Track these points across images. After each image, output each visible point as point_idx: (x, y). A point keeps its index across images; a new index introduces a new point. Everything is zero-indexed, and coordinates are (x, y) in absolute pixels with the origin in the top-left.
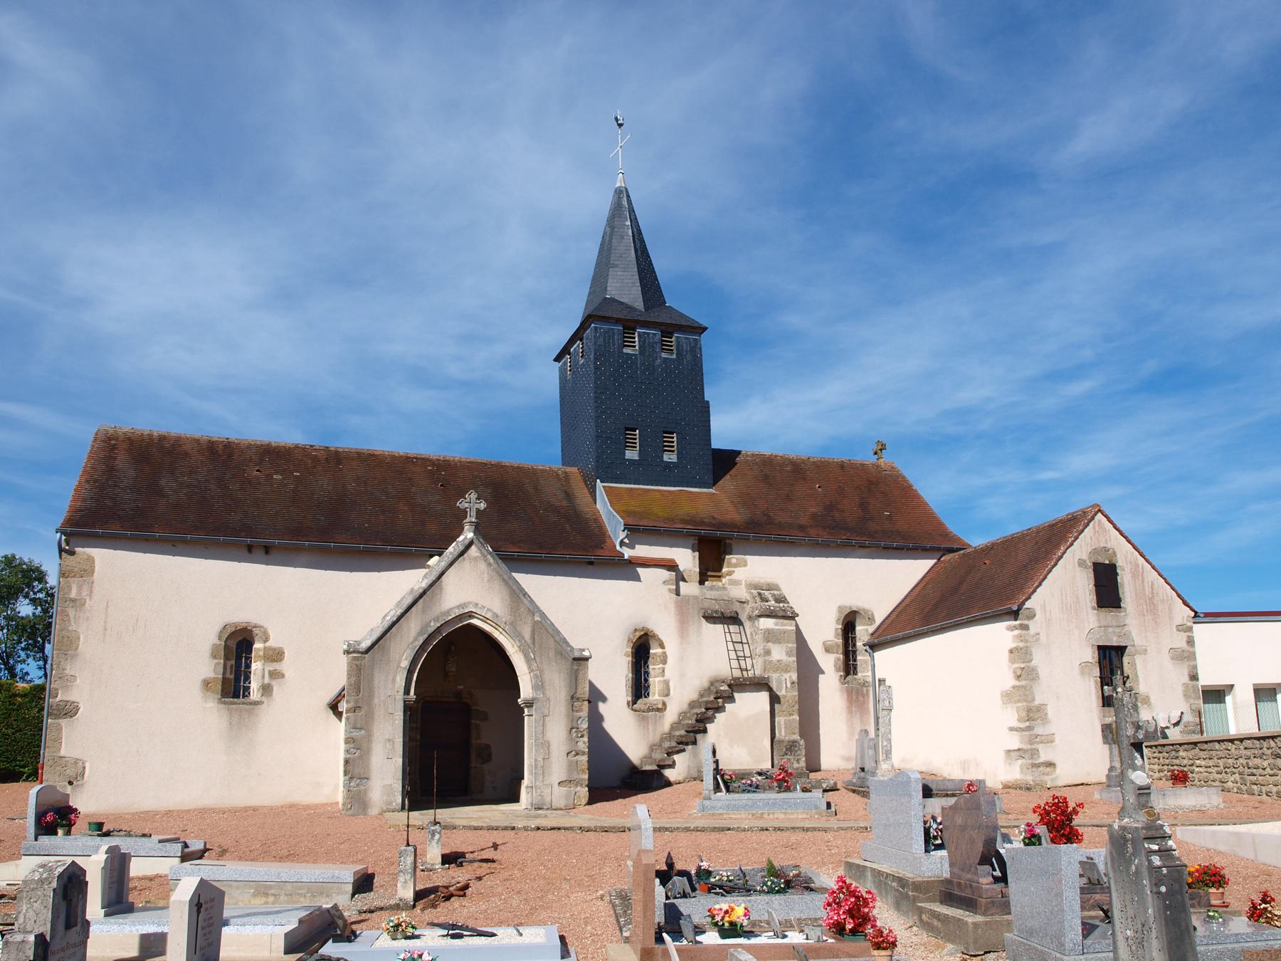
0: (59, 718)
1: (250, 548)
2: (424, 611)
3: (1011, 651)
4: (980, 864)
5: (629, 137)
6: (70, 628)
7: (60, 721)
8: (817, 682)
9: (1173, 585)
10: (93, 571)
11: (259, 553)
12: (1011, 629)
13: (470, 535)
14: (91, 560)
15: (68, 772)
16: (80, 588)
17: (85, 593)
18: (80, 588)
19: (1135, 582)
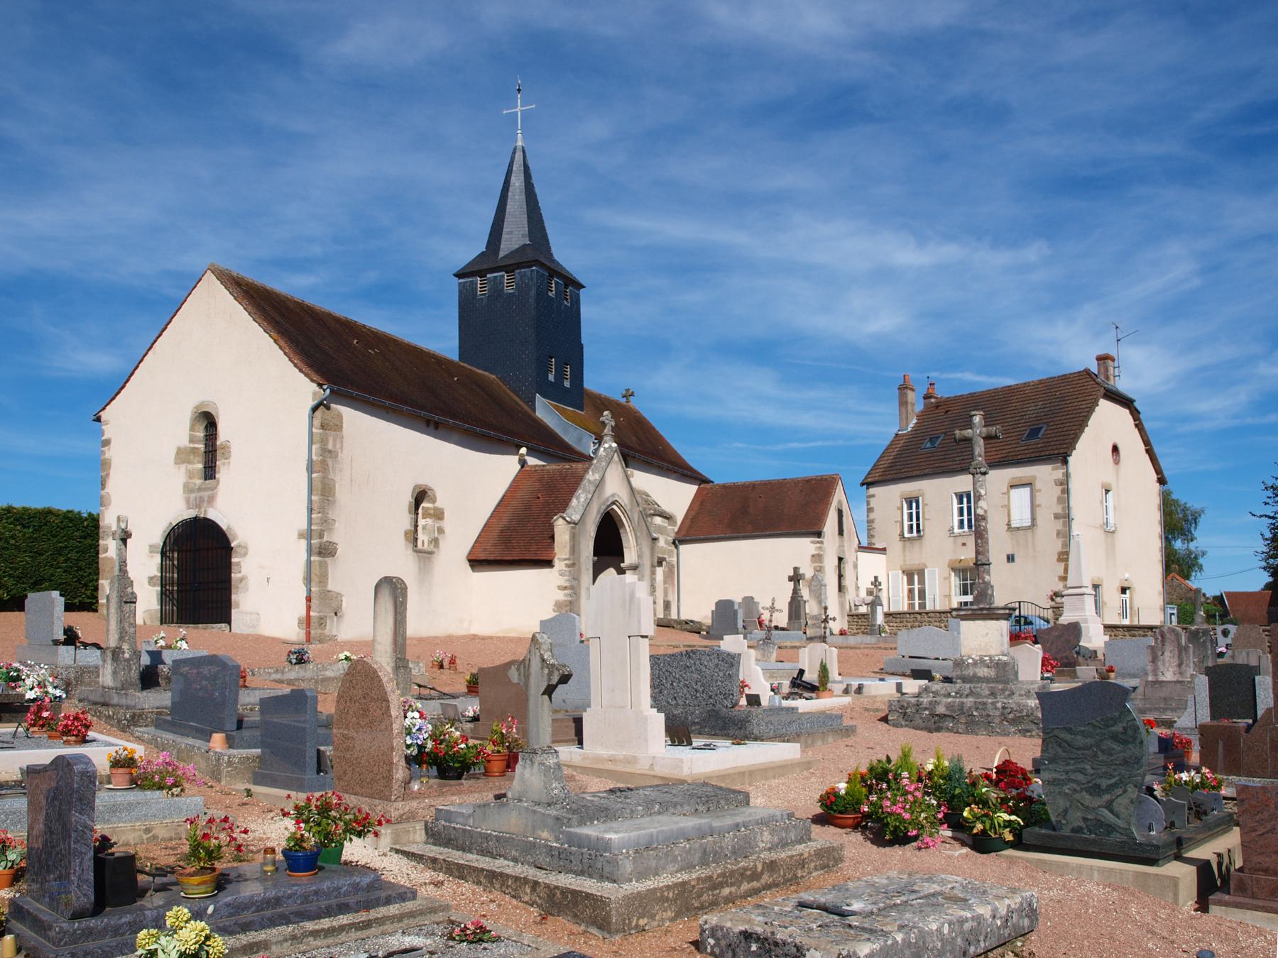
0: (325, 557)
1: (428, 423)
2: (598, 498)
3: (813, 556)
4: (819, 820)
5: (533, 106)
6: (330, 477)
7: (327, 559)
8: (1090, 410)
9: (152, 342)
10: (342, 427)
11: (432, 427)
12: (813, 542)
13: (1173, 624)
14: (340, 416)
15: (333, 605)
16: (335, 440)
17: (338, 446)
18: (335, 440)
19: (905, 556)
